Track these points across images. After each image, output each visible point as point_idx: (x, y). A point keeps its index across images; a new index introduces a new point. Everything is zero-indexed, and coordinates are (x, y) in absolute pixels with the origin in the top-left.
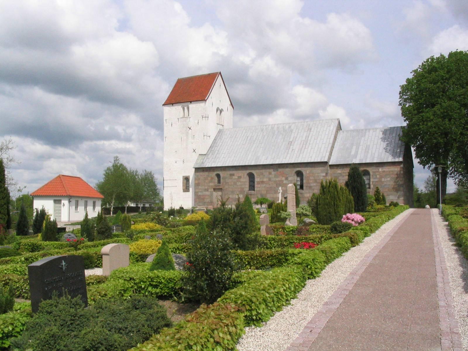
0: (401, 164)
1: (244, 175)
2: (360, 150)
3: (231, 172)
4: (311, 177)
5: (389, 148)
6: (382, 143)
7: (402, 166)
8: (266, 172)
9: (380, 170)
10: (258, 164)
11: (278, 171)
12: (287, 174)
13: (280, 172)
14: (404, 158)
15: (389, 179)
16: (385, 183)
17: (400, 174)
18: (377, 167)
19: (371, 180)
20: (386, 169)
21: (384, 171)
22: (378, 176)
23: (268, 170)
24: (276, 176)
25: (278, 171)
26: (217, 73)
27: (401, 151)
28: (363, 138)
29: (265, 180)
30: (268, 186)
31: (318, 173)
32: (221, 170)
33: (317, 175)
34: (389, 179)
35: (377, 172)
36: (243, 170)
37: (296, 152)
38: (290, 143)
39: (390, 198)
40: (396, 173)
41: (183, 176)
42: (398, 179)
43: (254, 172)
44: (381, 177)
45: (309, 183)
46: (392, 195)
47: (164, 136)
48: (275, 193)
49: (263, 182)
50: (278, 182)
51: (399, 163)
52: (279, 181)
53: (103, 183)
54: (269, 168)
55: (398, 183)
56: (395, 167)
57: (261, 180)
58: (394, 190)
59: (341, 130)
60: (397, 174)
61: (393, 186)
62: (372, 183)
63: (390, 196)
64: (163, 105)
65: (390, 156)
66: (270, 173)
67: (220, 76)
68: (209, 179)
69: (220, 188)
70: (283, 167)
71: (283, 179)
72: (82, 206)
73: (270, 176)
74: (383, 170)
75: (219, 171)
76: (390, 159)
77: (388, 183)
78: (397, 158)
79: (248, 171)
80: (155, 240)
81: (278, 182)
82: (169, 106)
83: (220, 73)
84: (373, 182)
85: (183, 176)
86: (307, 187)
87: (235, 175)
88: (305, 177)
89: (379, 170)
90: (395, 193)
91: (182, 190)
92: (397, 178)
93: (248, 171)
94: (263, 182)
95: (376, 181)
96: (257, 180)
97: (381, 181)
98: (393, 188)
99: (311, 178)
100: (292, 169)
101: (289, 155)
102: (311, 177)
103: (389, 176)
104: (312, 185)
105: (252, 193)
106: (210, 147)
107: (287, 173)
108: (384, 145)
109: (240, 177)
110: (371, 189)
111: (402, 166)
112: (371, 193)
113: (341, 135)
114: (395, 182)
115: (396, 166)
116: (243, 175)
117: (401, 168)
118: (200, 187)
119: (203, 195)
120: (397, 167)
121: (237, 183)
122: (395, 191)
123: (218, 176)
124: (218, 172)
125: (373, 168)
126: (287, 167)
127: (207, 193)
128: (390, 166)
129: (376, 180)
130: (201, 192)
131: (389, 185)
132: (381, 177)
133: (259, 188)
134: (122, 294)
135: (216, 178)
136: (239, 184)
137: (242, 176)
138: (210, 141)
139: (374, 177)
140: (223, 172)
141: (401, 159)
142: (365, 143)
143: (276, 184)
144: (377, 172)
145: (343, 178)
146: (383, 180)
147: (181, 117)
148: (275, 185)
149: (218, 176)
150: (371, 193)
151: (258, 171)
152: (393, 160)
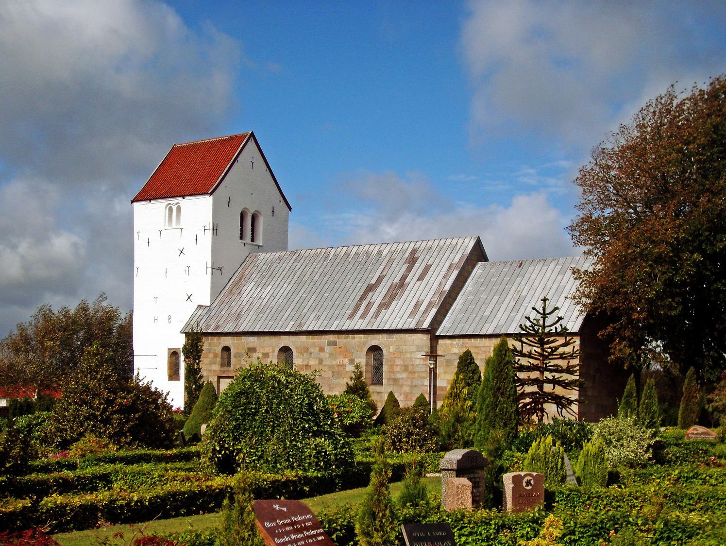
1: (273, 352)
4: (397, 360)
26: (242, 137)
31: (411, 353)
33: (408, 355)
45: (394, 372)
50: (337, 369)
53: (606, 273)
57: (306, 363)
59: (486, 260)
64: (132, 202)
67: (251, 143)
69: (231, 375)
71: (346, 361)
72: (439, 387)
73: (322, 355)
80: (509, 520)
81: (337, 369)
83: (252, 135)
85: (169, 349)
86: (389, 379)
88: (387, 359)
91: (167, 377)
99: (399, 362)
102: (397, 360)
104: (399, 376)
107: (353, 350)
113: (479, 269)
116: (271, 351)
137: (270, 354)
142: (519, 292)
148: (331, 373)
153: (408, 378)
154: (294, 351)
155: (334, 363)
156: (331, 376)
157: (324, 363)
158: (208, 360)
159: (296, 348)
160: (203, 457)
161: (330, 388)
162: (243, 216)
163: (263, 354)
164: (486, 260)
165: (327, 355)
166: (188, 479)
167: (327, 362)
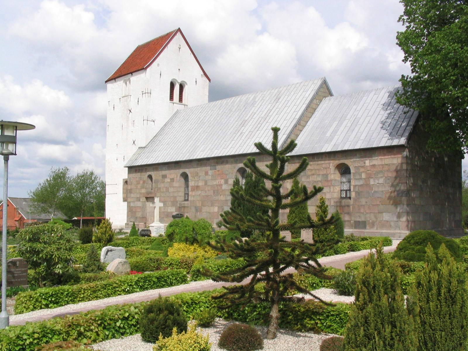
0: (404, 151)
2: (341, 129)
3: (164, 172)
5: (389, 121)
6: (382, 112)
7: (406, 153)
8: (201, 170)
9: (368, 162)
10: (191, 158)
11: (216, 169)
12: (227, 174)
13: (218, 171)
14: (409, 139)
15: (381, 181)
16: (376, 189)
17: (401, 170)
18: (362, 157)
19: (353, 183)
20: (377, 161)
21: (374, 166)
22: (364, 176)
23: (205, 169)
24: (214, 178)
25: (216, 169)
27: (407, 125)
28: (355, 107)
29: (201, 184)
30: (203, 194)
32: (154, 170)
34: (381, 181)
35: (362, 167)
36: (176, 169)
37: (244, 136)
38: (244, 124)
39: (384, 219)
40: (394, 168)
41: (124, 180)
42: (397, 181)
43: (187, 171)
44: (369, 177)
46: (387, 211)
47: (107, 125)
48: (212, 206)
49: (197, 187)
51: (400, 148)
52: (217, 185)
54: (205, 165)
55: (398, 189)
56: (392, 156)
58: (391, 202)
59: (331, 95)
60: (397, 171)
61: (387, 195)
62: (354, 188)
63: (384, 214)
64: (106, 82)
65: (386, 135)
66: (206, 173)
68: (141, 182)
70: (222, 163)
71: (223, 181)
74: (371, 164)
75: (151, 171)
76: (384, 141)
77: (380, 189)
78: (397, 138)
79: (181, 171)
82: (112, 83)
83: (179, 30)
84: (355, 186)
85: (123, 180)
87: (168, 177)
89: (365, 163)
90: (392, 208)
92: (396, 178)
93: (337, 162)
94: (197, 187)
95: (361, 185)
96: (191, 183)
97: (367, 185)
98: (390, 198)
100: (233, 165)
101: (233, 142)
103: (382, 176)
105: (186, 205)
106: (155, 136)
107: (227, 173)
108: (383, 115)
109: (172, 180)
110: (352, 199)
111: (406, 153)
112: (463, 203)
113: (326, 103)
114: (392, 186)
115: (394, 154)
116: (176, 176)
117: (403, 158)
118: (132, 195)
119: (135, 207)
120: (396, 156)
121: (170, 189)
122: (392, 204)
123: (185, 176)
124: (342, 161)
125: (354, 160)
126: (227, 163)
127: (139, 204)
128: (384, 155)
129: (361, 183)
130: (133, 202)
131: (382, 191)
132: (369, 177)
133: (194, 196)
134: (22, 348)
135: (183, 180)
136: (171, 190)
138: (155, 129)
139: (358, 177)
140: (155, 172)
141: (403, 141)
142: (354, 116)
143: (214, 191)
144: (362, 167)
145: (308, 180)
146: (372, 182)
147: (123, 96)
148: (212, 191)
149: (185, 176)
150: (351, 207)
151: (192, 170)
152: (389, 143)
153: (359, 273)
154: (189, 175)
155: (215, 183)
156: (212, 194)
157: (208, 184)
158: (140, 185)
159: (191, 173)
160: (288, 295)
161: (212, 204)
162: (172, 85)
163: (171, 179)
164: (331, 95)
165: (210, 177)
166: (441, 338)
167: (210, 183)
